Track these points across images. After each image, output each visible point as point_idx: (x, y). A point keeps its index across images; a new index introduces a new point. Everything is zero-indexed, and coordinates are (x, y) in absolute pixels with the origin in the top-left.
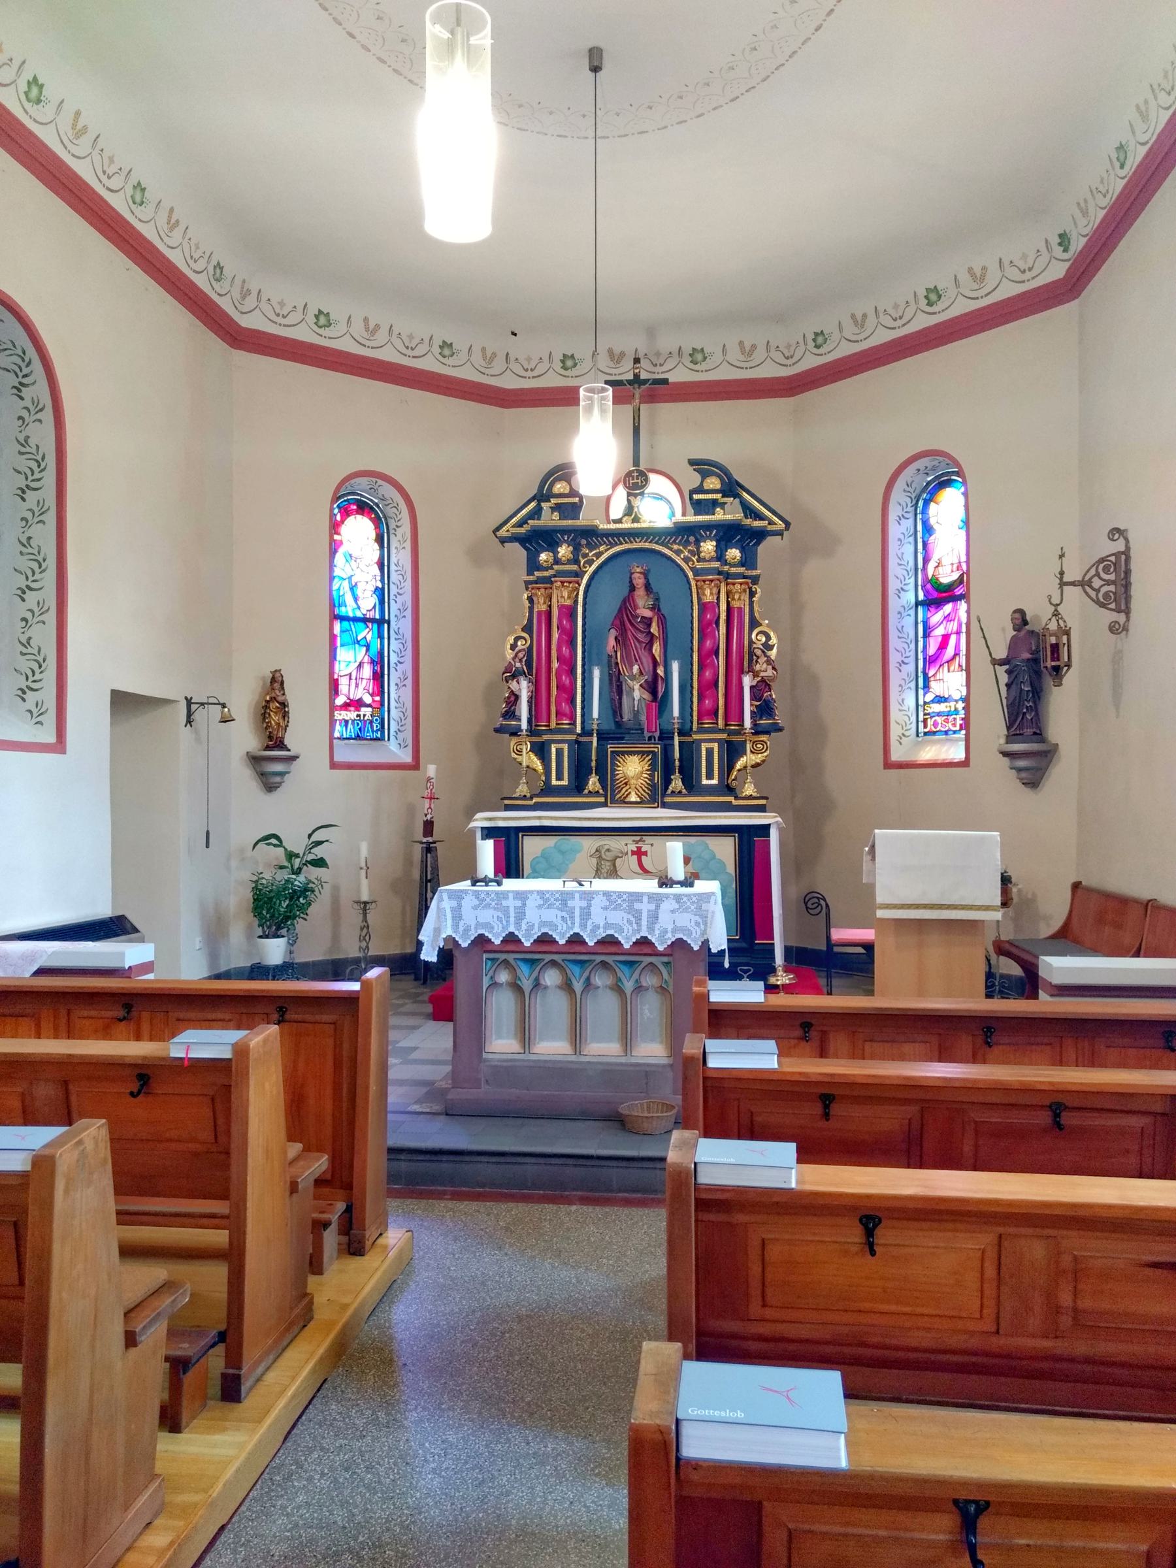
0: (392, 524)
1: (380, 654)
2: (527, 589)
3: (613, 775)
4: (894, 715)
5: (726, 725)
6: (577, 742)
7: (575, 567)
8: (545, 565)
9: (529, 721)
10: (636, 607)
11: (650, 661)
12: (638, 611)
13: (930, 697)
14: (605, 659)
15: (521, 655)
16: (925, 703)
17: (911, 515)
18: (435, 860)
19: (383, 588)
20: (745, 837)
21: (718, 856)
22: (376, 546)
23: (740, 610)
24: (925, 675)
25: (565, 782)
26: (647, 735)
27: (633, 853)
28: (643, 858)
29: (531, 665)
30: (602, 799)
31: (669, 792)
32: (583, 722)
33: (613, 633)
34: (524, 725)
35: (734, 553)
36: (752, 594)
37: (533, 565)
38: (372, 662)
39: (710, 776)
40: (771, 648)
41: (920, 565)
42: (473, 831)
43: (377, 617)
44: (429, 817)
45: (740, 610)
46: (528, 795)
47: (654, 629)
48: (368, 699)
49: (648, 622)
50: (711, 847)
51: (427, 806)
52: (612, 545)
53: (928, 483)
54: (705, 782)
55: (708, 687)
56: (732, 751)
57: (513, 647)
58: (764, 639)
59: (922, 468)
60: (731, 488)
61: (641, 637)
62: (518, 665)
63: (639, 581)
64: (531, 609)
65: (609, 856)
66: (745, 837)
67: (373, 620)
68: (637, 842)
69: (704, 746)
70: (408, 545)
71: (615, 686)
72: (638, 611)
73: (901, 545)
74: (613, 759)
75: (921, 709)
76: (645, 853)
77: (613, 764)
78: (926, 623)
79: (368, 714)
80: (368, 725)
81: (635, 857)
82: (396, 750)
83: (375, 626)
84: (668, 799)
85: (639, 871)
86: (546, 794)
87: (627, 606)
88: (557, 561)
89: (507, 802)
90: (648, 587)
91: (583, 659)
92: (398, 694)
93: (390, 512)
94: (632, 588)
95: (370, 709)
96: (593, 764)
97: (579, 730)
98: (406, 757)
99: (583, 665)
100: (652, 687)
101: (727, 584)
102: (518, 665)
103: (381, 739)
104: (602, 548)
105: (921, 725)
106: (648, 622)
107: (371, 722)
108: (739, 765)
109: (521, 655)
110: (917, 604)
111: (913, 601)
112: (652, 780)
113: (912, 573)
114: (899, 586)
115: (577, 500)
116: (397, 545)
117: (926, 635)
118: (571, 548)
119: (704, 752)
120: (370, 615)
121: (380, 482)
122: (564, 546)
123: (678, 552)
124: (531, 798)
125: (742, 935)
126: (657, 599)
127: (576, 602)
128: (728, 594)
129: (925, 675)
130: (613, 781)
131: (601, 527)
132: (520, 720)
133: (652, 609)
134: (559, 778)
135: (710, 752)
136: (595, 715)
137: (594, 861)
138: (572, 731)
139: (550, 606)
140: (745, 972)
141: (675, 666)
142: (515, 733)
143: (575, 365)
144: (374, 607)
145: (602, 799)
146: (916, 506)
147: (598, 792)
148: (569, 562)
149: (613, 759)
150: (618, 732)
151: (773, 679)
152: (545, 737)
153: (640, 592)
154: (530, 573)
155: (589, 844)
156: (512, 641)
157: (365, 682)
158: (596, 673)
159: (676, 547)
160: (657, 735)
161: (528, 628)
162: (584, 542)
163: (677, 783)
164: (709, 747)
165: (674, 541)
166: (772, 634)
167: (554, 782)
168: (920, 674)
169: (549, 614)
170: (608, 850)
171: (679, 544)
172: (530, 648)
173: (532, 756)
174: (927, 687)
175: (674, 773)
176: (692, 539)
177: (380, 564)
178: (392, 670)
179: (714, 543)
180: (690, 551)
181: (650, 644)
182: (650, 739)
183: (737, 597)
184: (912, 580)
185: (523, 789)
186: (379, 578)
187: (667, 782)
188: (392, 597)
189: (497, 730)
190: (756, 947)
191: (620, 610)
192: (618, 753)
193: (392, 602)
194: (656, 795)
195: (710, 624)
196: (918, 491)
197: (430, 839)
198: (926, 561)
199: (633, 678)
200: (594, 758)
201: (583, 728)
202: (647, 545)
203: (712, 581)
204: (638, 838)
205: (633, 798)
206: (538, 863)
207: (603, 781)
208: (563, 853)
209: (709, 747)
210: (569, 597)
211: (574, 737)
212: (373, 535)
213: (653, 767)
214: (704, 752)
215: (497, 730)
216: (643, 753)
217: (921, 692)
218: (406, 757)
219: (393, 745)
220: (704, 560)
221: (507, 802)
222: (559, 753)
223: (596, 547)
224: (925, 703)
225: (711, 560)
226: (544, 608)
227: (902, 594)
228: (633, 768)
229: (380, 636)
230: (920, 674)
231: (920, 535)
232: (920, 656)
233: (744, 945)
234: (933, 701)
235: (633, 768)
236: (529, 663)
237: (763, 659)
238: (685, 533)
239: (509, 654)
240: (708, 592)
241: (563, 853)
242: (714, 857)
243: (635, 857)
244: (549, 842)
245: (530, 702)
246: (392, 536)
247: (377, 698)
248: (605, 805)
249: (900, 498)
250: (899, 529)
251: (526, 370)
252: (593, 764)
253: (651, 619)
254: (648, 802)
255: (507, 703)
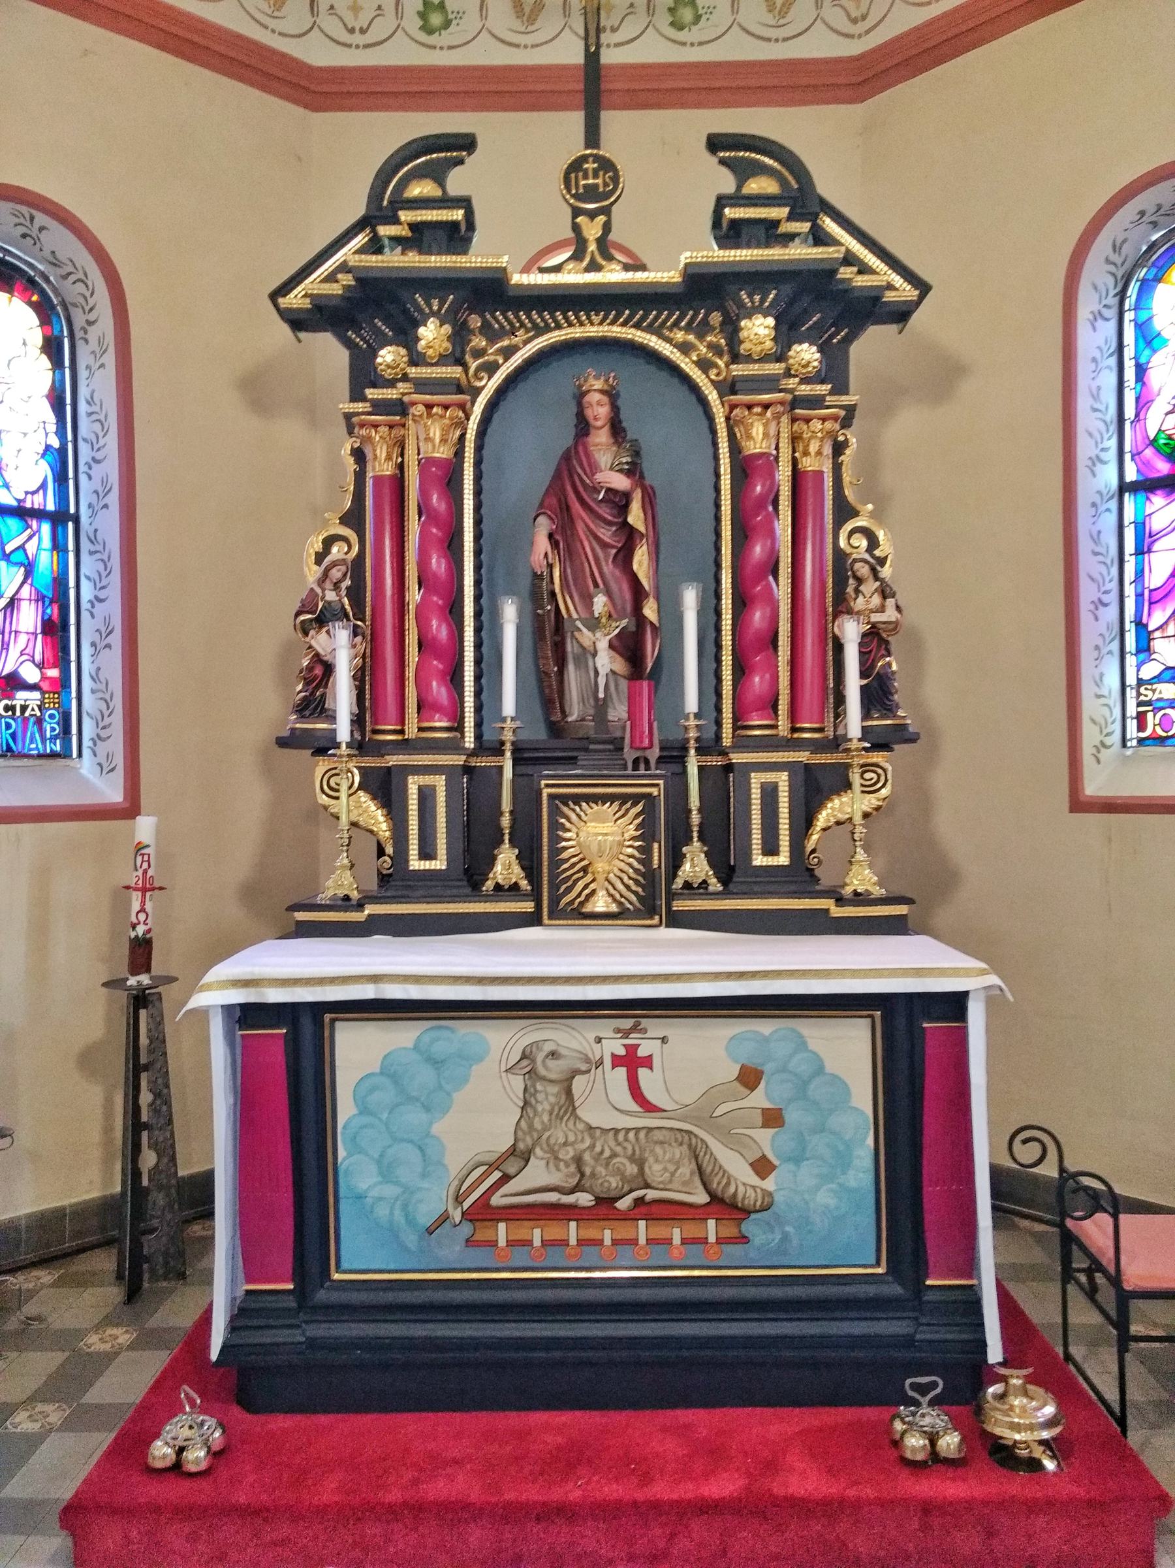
0: (79, 319)
1: (59, 582)
2: (350, 433)
3: (555, 851)
4: (1089, 706)
5: (794, 730)
6: (467, 770)
7: (455, 372)
8: (388, 374)
9: (358, 721)
10: (594, 468)
11: (625, 587)
12: (599, 477)
13: (1150, 670)
14: (525, 583)
15: (336, 574)
16: (1140, 682)
17: (1112, 313)
18: (158, 1023)
19: (62, 451)
20: (901, 1022)
21: (829, 1067)
22: (45, 362)
23: (819, 474)
24: (1140, 624)
25: (439, 864)
26: (629, 755)
27: (617, 1061)
28: (642, 1072)
29: (356, 598)
30: (528, 907)
31: (678, 883)
32: (478, 725)
33: (544, 526)
34: (344, 731)
35: (806, 354)
36: (839, 448)
37: (363, 374)
38: (40, 598)
39: (771, 849)
40: (882, 561)
41: (1130, 411)
42: (202, 1014)
43: (51, 507)
44: (140, 930)
45: (819, 474)
46: (355, 895)
47: (636, 517)
48: (30, 674)
49: (620, 502)
50: (813, 1045)
51: (136, 906)
52: (540, 331)
53: (1153, 247)
54: (759, 860)
55: (752, 650)
56: (815, 787)
57: (319, 558)
58: (864, 543)
59: (1151, 209)
60: (805, 201)
61: (606, 534)
62: (331, 596)
63: (599, 410)
64: (360, 477)
65: (555, 1069)
66: (901, 1022)
67: (40, 514)
68: (626, 1034)
69: (757, 780)
70: (110, 359)
71: (550, 639)
72: (599, 477)
73: (1097, 371)
74: (555, 812)
75: (1131, 694)
76: (648, 1062)
77: (555, 826)
78: (1141, 527)
79: (34, 704)
80: (32, 728)
81: (622, 1072)
82: (94, 778)
83: (46, 527)
84: (679, 905)
85: (634, 1107)
86: (396, 899)
87: (571, 467)
88: (416, 359)
89: (301, 916)
90: (617, 429)
91: (478, 583)
92: (96, 662)
93: (71, 291)
94: (583, 427)
95: (36, 695)
96: (506, 821)
97: (469, 741)
98: (113, 793)
99: (478, 598)
100: (630, 647)
101: (794, 420)
102: (331, 596)
103: (65, 754)
104: (521, 335)
105: (1132, 725)
106: (620, 502)
107: (39, 722)
108: (823, 818)
109: (336, 574)
110: (1124, 488)
111: (1114, 482)
112: (646, 861)
113: (1113, 428)
114: (1093, 452)
115: (458, 215)
116: (90, 360)
117: (1142, 550)
118: (447, 329)
119: (756, 793)
120: (36, 501)
121: (41, 219)
122: (432, 323)
123: (685, 348)
124: (360, 906)
125: (893, 1268)
126: (637, 454)
127: (459, 453)
128: (795, 439)
129: (1140, 624)
130: (555, 863)
131: (517, 278)
132: (332, 718)
133: (629, 473)
134: (427, 853)
135: (769, 793)
136: (509, 706)
137: (517, 1083)
138: (454, 746)
139: (401, 467)
140: (923, 1389)
141: (690, 598)
142: (324, 747)
143: (447, 24)
144: (43, 486)
145: (528, 907)
146: (1122, 295)
147: (515, 887)
148: (443, 360)
149: (555, 812)
150: (557, 743)
151: (895, 627)
152: (393, 760)
153: (601, 437)
154: (357, 395)
155: (503, 1040)
156: (318, 547)
157: (23, 639)
158: (510, 613)
159: (679, 336)
160: (654, 754)
161: (354, 518)
162: (475, 321)
163: (696, 865)
164: (768, 780)
165: (676, 324)
166: (881, 535)
167: (416, 864)
168: (1130, 627)
169: (398, 482)
170: (553, 1054)
171: (688, 328)
172: (358, 564)
173: (363, 797)
174: (1145, 649)
175: (688, 840)
176: (716, 318)
177: (56, 400)
178: (85, 615)
179: (771, 321)
180: (710, 346)
181: (625, 556)
182: (636, 762)
183: (813, 447)
184: (1113, 443)
185: (340, 881)
186: (52, 428)
187: (675, 860)
188: (82, 468)
189: (282, 743)
190: (929, 1297)
191: (557, 476)
192: (565, 799)
193: (83, 478)
194: (654, 900)
195: (761, 504)
196: (1128, 265)
197: (145, 979)
198: (1143, 403)
199: (594, 624)
200: (506, 805)
201: (478, 737)
202: (617, 331)
203: (766, 406)
204: (627, 1024)
205: (601, 904)
206: (373, 1089)
207: (529, 863)
208: (436, 1063)
209: (768, 780)
210: (444, 441)
211: (459, 760)
212: (37, 337)
213: (647, 833)
214: (756, 793)
215: (282, 743)
216: (624, 799)
217: (1131, 661)
218: (113, 793)
219: (86, 766)
220: (749, 359)
221: (301, 916)
222: (426, 796)
223: (501, 334)
224: (1140, 682)
225: (765, 359)
226: (388, 470)
227: (1099, 467)
228: (601, 836)
229: (58, 546)
230: (1130, 627)
231: (1129, 353)
232: (1130, 590)
233: (897, 1290)
234: (1158, 678)
235: (601, 836)
236: (356, 594)
237: (870, 587)
238: (705, 291)
239: (313, 573)
240: (758, 430)
241: (436, 1063)
242: (820, 1070)
243: (622, 1072)
244: (402, 1036)
245: (359, 677)
246: (80, 344)
247: (53, 673)
248: (534, 919)
249: (1097, 275)
250: (1094, 339)
251: (352, 31)
252: (506, 821)
253: (627, 497)
254: (637, 914)
255: (307, 683)
